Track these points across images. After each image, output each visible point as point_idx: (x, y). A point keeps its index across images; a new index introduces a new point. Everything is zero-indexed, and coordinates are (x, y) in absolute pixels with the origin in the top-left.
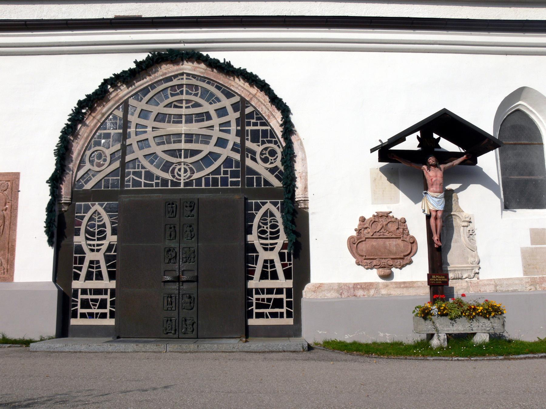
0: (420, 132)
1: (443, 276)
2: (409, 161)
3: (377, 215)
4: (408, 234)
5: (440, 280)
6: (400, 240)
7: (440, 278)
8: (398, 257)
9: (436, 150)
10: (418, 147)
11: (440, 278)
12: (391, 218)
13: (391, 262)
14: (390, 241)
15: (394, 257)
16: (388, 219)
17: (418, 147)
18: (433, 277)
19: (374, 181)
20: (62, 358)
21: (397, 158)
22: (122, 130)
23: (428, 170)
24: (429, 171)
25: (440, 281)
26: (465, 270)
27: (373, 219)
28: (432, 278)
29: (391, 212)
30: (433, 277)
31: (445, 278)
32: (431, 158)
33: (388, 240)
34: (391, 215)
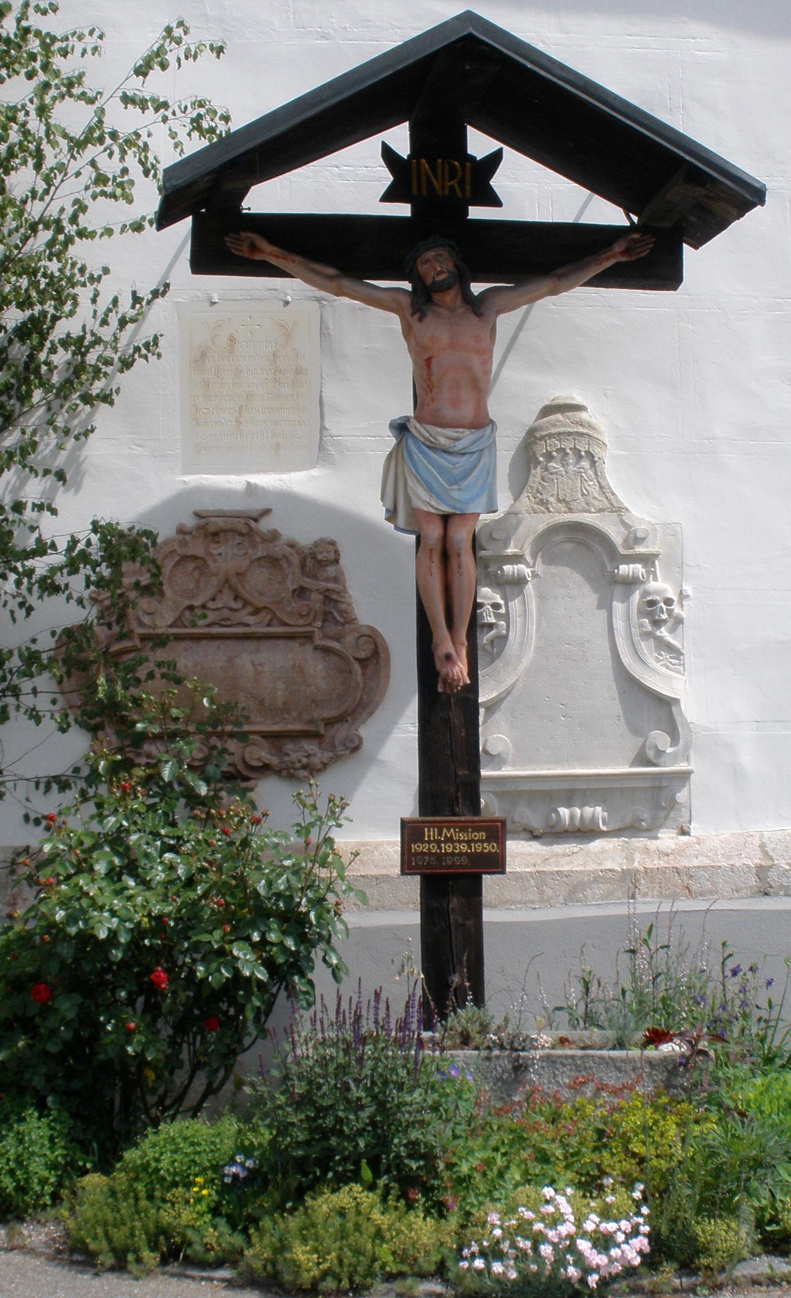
0: (412, 129)
1: (477, 829)
2: (331, 271)
3: (200, 528)
4: (349, 620)
5: (464, 848)
6: (309, 647)
7: (460, 842)
8: (297, 727)
9: (476, 213)
10: (390, 196)
11: (460, 842)
12: (264, 540)
13: (260, 753)
14: (258, 650)
15: (275, 728)
16: (254, 545)
17: (390, 196)
18: (430, 833)
19: (196, 361)
20: (258, 814)
21: (270, 254)
22: (471, 216)
23: (417, 316)
24: (420, 320)
25: (461, 854)
26: (622, 790)
27: (176, 546)
28: (423, 842)
29: (266, 512)
30: (430, 833)
31: (488, 840)
32: (431, 254)
33: (250, 645)
34: (265, 525)
